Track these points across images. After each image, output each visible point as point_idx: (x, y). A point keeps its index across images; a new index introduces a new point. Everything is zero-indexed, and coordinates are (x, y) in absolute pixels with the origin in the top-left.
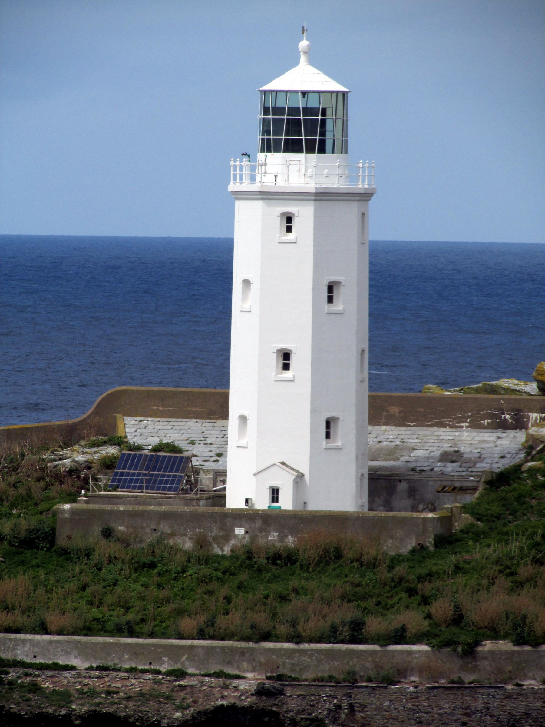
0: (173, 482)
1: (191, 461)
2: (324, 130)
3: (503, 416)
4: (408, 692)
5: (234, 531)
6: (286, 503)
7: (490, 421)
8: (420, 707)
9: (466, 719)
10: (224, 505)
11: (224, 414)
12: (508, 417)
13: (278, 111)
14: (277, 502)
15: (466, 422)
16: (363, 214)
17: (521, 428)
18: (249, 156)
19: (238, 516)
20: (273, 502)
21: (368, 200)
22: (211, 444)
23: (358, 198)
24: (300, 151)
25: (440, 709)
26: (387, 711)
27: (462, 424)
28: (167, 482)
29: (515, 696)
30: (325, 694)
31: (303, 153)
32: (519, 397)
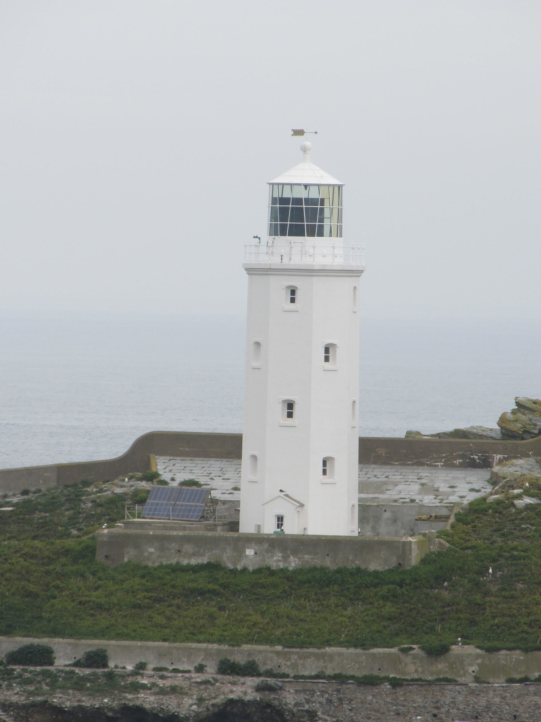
1: (210, 493)
2: (322, 217)
6: (291, 528)
7: (461, 461)
8: (398, 701)
9: (436, 711)
10: (237, 530)
11: (239, 456)
12: (476, 457)
16: (355, 288)
17: (487, 467)
18: (259, 238)
19: (249, 539)
21: (359, 276)
22: (229, 479)
24: (303, 235)
25: (415, 703)
26: (369, 704)
27: (438, 464)
28: (190, 511)
29: (477, 693)
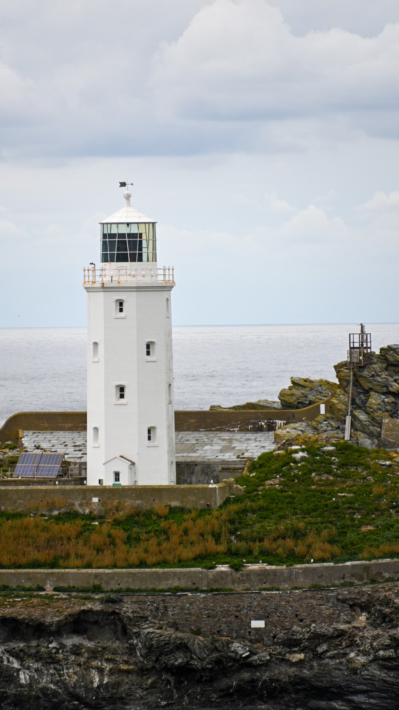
0: (49, 471)
3: (260, 423)
4: (201, 598)
5: (91, 500)
6: (125, 481)
7: (252, 426)
11: (85, 428)
12: (263, 423)
13: (112, 236)
14: (119, 480)
15: (237, 427)
19: (95, 491)
20: (116, 481)
21: (170, 290)
23: (136, 290)
27: (235, 429)
29: (268, 598)
30: (149, 600)
31: (128, 261)
32: (269, 411)
